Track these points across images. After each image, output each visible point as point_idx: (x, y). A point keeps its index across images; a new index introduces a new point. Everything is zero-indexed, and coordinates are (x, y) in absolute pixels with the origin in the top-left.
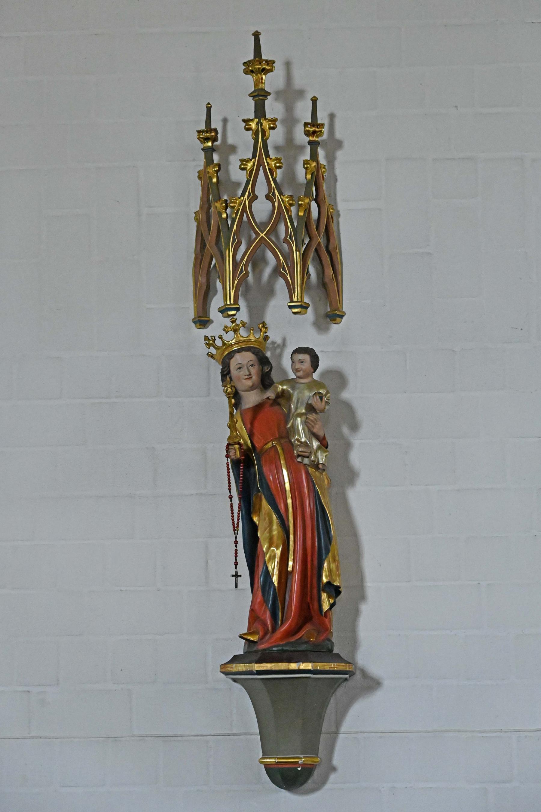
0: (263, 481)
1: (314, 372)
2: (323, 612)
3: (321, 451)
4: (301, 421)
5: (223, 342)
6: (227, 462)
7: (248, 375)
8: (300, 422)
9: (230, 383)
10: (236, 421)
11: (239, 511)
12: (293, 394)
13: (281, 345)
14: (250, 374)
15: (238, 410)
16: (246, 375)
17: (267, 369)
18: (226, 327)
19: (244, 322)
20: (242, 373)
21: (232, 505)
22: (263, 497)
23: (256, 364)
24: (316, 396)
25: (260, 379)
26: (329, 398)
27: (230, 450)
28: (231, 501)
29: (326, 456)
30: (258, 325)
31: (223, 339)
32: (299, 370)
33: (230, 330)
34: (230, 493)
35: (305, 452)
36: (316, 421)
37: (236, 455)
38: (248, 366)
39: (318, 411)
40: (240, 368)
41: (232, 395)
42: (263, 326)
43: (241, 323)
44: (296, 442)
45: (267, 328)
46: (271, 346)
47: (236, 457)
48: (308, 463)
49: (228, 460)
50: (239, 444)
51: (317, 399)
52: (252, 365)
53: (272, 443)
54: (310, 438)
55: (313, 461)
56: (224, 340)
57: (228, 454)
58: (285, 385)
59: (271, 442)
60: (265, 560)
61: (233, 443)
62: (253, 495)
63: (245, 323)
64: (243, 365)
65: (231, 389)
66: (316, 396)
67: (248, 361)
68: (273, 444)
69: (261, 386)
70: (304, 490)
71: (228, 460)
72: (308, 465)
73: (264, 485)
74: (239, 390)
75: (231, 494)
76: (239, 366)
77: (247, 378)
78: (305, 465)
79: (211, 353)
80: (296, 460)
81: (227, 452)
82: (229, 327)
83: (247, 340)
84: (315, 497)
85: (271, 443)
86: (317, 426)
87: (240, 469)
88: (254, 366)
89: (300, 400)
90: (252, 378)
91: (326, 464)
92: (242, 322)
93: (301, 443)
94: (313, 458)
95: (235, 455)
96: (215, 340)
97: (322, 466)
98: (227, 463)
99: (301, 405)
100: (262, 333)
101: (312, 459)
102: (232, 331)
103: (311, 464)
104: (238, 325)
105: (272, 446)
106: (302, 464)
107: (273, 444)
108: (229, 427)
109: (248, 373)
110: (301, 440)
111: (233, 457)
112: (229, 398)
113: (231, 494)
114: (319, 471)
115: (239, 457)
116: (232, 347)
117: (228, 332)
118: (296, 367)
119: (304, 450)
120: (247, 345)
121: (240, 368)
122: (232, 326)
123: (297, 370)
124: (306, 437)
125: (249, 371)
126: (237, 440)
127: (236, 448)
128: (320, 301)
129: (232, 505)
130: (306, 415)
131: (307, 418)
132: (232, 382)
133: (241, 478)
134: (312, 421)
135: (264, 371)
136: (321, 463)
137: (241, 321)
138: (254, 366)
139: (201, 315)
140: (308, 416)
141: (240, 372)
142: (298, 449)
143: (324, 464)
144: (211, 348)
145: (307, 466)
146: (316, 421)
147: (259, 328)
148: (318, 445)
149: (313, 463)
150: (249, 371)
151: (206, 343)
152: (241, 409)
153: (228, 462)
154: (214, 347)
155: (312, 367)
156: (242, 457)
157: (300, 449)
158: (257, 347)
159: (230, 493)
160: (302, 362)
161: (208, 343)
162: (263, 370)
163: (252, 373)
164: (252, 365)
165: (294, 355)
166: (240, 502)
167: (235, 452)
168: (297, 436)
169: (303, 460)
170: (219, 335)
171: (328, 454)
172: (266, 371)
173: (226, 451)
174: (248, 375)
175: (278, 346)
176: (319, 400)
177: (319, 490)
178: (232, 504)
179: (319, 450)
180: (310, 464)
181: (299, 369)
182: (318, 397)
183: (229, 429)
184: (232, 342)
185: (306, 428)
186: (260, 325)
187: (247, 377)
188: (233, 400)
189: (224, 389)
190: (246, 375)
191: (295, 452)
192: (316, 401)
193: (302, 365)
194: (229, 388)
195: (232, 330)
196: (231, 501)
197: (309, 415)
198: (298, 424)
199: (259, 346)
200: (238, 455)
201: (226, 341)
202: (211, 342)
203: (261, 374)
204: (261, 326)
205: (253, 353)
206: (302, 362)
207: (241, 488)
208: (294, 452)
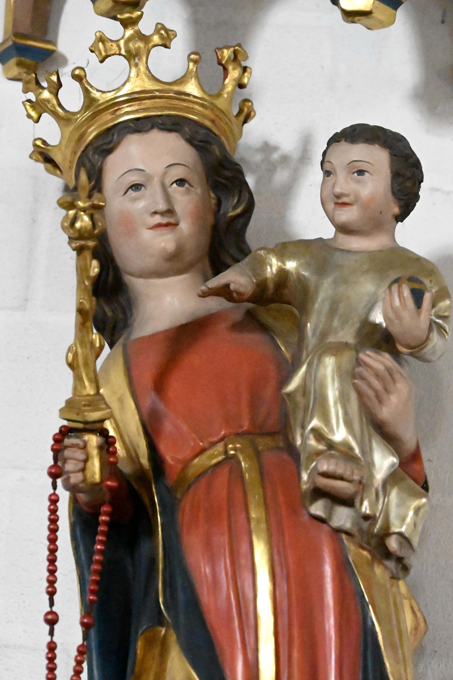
0: (179, 582)
1: (401, 217)
2: (285, 389)
3: (400, 489)
4: (338, 368)
5: (86, 92)
6: (52, 491)
7: (162, 214)
8: (333, 372)
9: (90, 196)
10: (98, 345)
11: (79, 663)
12: (317, 288)
13: (296, 155)
14: (170, 212)
15: (118, 347)
16: (155, 213)
17: (235, 207)
18: (102, 39)
19: (167, 31)
20: (141, 204)
21: (52, 647)
22: (173, 638)
23: (193, 178)
24: (399, 286)
25: (205, 240)
26: (446, 314)
27: (67, 453)
28: (51, 633)
29: (417, 511)
30: (219, 49)
31: (89, 84)
32: (345, 200)
33: (115, 48)
34: (52, 603)
35: (341, 478)
36: (393, 378)
37: (89, 475)
38: (168, 181)
39: (401, 349)
40: (136, 187)
41: (91, 244)
42: (235, 58)
43: (157, 31)
44: (312, 442)
45: (248, 70)
46: (258, 158)
47: (84, 480)
48: (348, 526)
49: (55, 486)
50: (104, 433)
51: (400, 295)
52: (181, 182)
53: (226, 446)
54: (366, 432)
55: (366, 518)
56: (91, 87)
57: (59, 464)
58: (292, 257)
59: (222, 443)
60: (95, 371)
61: (80, 426)
62: (137, 632)
63: (170, 33)
64: (149, 178)
65: (92, 217)
66: (399, 286)
67: (169, 166)
68: (226, 452)
69: (207, 262)
70: (322, 623)
71: (55, 486)
72: (347, 533)
73: (181, 597)
74: (132, 274)
75: (54, 609)
76: (134, 178)
77: (159, 226)
78: (338, 531)
79: (44, 142)
80: (306, 509)
81: (56, 459)
82: (112, 41)
83: (172, 91)
84: (365, 650)
85: (220, 447)
86: (394, 399)
87: (96, 533)
88: (187, 185)
89: (342, 308)
90: (178, 227)
91: (415, 541)
92: (161, 29)
93: (331, 445)
94: (366, 508)
95: (83, 470)
96: (60, 85)
97: (400, 544)
98: (51, 495)
99: (345, 321)
100: (227, 81)
101: (363, 509)
102: (120, 54)
103: (360, 530)
104: (145, 39)
105: (224, 460)
106: (325, 525)
107: (226, 452)
108: (71, 365)
109: (162, 206)
110: (330, 437)
111: (76, 478)
112: (80, 250)
113: (54, 609)
114: (386, 567)
115: (97, 478)
116: (118, 113)
117: (109, 56)
118: (338, 190)
119: (340, 470)
120: (170, 109)
121: (136, 187)
122: (123, 38)
123: (340, 201)
124: (348, 424)
125: (168, 198)
126: (95, 416)
127: (88, 446)
128: (443, 22)
129: (52, 647)
130: (357, 352)
131: (359, 362)
132: (96, 195)
133: (99, 547)
134: (377, 375)
135: (222, 212)
136: (397, 530)
137: (158, 23)
138: (191, 185)
139: (25, 28)
140: (362, 356)
141: (136, 199)
142: (316, 465)
143: (407, 535)
144: (46, 116)
145: (344, 536)
146: (393, 378)
147: (220, 63)
148: (393, 465)
149: (365, 525)
150: (168, 198)
151: (29, 101)
152: (127, 339)
153: (54, 494)
154: (54, 114)
155: (393, 193)
156: (109, 483)
157: (324, 466)
158: (208, 123)
159: (52, 603)
160: (361, 172)
161: (34, 99)
162: (219, 210)
163: (178, 208)
164: (181, 182)
165: (335, 146)
166: (86, 636)
167: (86, 461)
168: (319, 420)
169: (330, 514)
170: (78, 68)
171: (424, 505)
172: (232, 214)
173: (51, 454)
174: (162, 214)
175: (285, 159)
176: (410, 303)
177: (378, 629)
178: (55, 643)
179: (392, 487)
180: (355, 531)
181: (347, 195)
182: (406, 292)
183: (69, 372)
184: (118, 95)
185: (353, 396)
186: (225, 51)
187: (158, 219)
188: (95, 263)
189: (67, 215)
190: (155, 213)
191: (305, 477)
192: (397, 302)
193: (358, 182)
194: (84, 210)
195: (123, 52)
196: (51, 633)
197: (368, 352)
198: (325, 377)
199: (213, 121)
200: (94, 473)
201: (98, 91)
202: (46, 95)
203: (210, 219)
204: (227, 53)
205: (190, 141)
206: (361, 172)
207: (93, 592)
208: (299, 477)
